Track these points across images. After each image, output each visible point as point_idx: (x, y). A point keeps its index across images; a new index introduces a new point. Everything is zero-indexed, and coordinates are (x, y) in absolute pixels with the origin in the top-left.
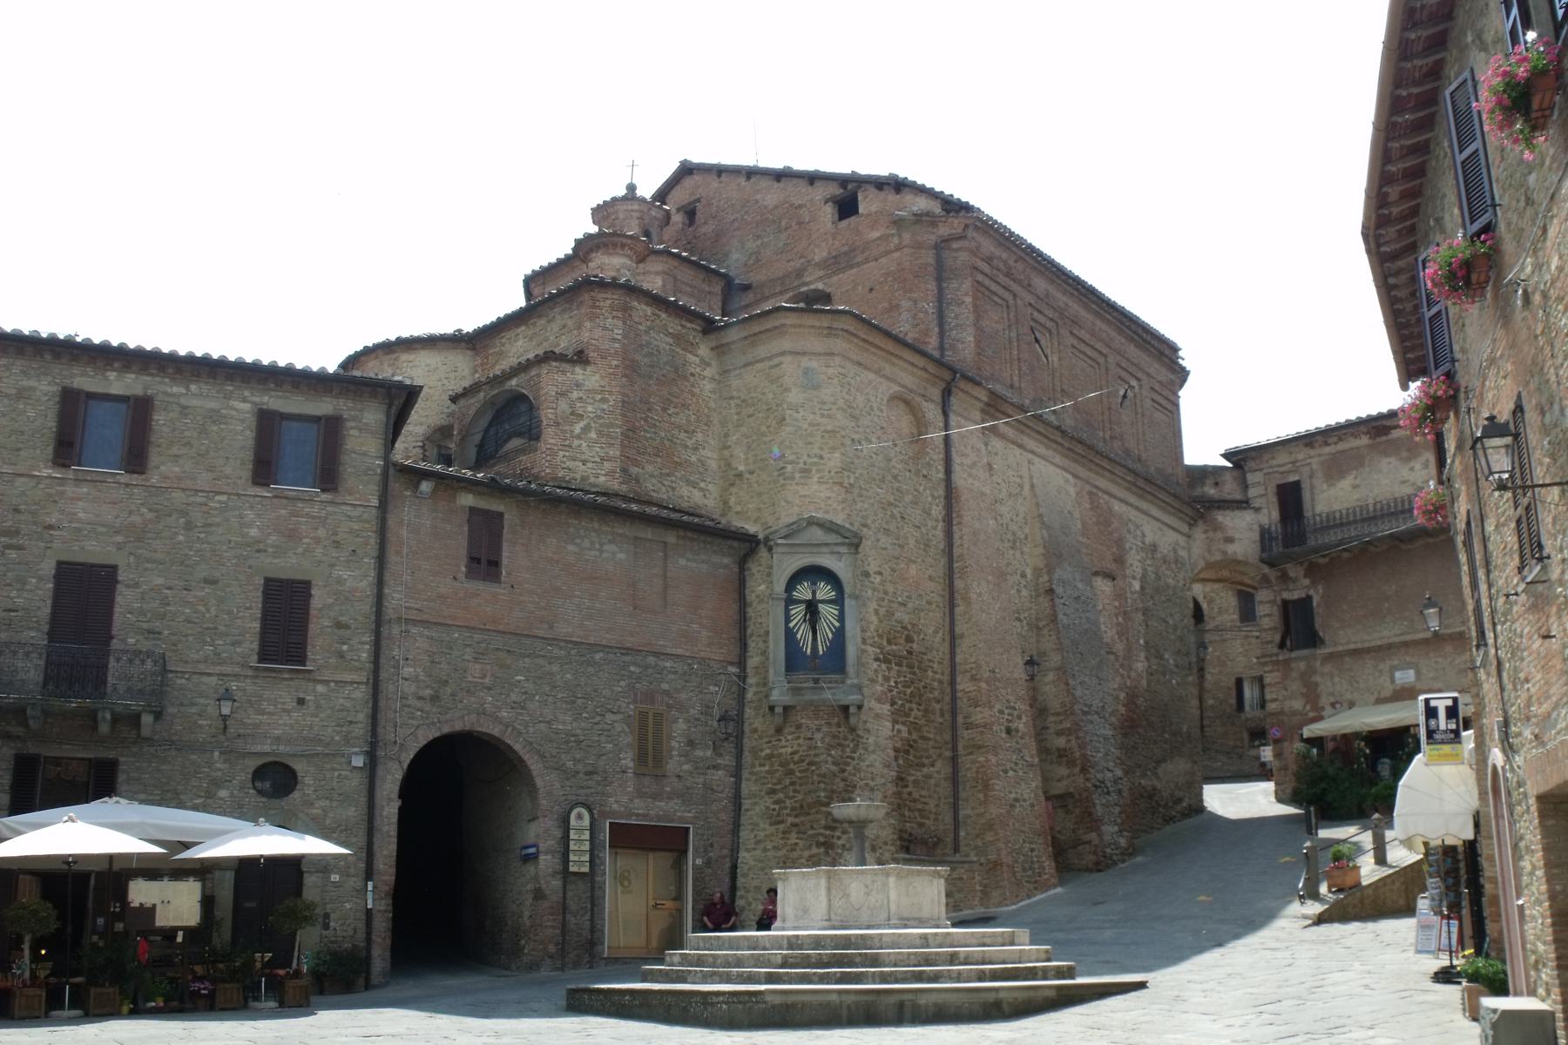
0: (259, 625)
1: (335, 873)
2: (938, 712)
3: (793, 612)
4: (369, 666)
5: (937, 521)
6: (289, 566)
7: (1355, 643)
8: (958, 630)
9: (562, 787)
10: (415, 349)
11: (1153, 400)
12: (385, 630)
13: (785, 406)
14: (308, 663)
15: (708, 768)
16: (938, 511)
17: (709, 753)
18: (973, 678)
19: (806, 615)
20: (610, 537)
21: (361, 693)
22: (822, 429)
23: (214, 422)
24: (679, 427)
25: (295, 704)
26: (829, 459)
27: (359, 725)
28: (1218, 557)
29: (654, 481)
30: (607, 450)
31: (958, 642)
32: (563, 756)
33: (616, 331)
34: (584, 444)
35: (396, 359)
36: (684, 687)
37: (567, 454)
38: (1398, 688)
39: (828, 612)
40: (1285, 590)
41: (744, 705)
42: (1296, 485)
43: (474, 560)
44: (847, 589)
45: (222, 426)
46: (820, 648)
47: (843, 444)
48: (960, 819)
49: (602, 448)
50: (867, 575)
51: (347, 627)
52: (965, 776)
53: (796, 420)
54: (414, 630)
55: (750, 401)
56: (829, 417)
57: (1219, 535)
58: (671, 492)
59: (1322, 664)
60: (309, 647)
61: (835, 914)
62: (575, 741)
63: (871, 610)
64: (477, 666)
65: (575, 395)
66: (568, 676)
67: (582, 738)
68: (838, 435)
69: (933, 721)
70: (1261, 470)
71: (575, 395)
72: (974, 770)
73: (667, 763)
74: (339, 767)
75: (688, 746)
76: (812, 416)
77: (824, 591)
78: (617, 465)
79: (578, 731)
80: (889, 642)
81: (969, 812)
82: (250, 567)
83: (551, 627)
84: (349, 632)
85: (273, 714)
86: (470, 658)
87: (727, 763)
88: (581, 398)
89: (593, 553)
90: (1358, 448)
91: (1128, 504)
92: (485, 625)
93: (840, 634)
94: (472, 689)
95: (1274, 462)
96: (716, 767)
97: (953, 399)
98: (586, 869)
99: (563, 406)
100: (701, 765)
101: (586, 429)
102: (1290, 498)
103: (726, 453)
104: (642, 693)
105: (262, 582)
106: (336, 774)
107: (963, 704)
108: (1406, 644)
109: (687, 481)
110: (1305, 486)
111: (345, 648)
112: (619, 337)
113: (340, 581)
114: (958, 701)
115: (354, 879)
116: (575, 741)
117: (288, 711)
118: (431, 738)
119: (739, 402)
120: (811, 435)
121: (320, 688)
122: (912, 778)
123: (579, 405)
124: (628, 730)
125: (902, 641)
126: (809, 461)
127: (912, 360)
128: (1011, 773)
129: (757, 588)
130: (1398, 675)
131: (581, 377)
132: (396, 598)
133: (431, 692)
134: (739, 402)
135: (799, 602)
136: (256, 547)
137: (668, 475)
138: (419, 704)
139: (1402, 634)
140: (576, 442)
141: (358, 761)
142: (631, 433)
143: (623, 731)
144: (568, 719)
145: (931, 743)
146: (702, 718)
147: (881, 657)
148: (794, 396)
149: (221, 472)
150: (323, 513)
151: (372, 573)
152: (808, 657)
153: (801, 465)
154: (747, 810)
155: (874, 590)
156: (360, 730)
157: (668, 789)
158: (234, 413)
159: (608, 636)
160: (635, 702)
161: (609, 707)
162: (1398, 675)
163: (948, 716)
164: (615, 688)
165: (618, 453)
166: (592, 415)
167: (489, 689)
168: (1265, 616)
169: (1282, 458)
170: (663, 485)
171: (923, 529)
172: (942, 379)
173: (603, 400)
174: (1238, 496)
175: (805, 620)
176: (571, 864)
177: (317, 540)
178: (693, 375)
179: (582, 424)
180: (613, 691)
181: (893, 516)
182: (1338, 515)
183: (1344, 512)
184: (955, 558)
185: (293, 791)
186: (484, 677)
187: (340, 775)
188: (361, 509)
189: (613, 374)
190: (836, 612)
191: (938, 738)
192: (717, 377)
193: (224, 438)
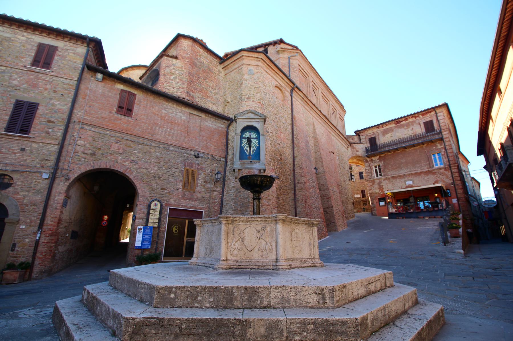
0: (8, 117)
1: (23, 225)
2: (290, 179)
3: (243, 141)
4: (61, 138)
5: (289, 124)
6: (29, 97)
7: (393, 175)
8: (295, 155)
9: (150, 193)
10: (134, 70)
12: (71, 125)
13: (243, 79)
14: (30, 134)
15: (212, 191)
16: (289, 121)
17: (212, 186)
18: (301, 168)
19: (247, 142)
20: (180, 111)
21: (55, 148)
22: (254, 86)
23: (7, 41)
24: (210, 86)
25: (19, 151)
26: (256, 95)
27: (51, 162)
28: (355, 155)
29: (199, 99)
30: (182, 85)
31: (295, 158)
32: (152, 182)
33: (188, 52)
34: (174, 82)
35: (129, 73)
36: (204, 163)
37: (167, 84)
38: (407, 186)
39: (254, 142)
41: (226, 171)
42: (374, 138)
43: (120, 107)
44: (261, 132)
45: (10, 43)
46: (252, 152)
47: (261, 92)
48: (297, 212)
49: (180, 84)
50: (268, 132)
51: (53, 122)
52: (298, 199)
53: (246, 83)
54: (87, 127)
55: (232, 81)
56: (257, 83)
57: (355, 150)
58: (205, 104)
59: (384, 181)
60: (32, 128)
61: (232, 255)
62: (158, 177)
63: (269, 143)
64: (116, 145)
65: (172, 67)
66: (158, 154)
67: (161, 176)
68: (259, 89)
69: (288, 181)
71: (172, 67)
72: (301, 196)
73: (196, 188)
74: (36, 178)
75: (204, 183)
76: (251, 83)
77: (254, 135)
78: (185, 90)
79: (160, 174)
80: (275, 154)
81: (300, 210)
82: (10, 95)
83: (152, 136)
84: (54, 124)
85: (7, 154)
86: (113, 142)
87: (219, 190)
88: (174, 69)
89: (173, 115)
90: (392, 127)
92: (122, 130)
93: (258, 148)
94: (113, 153)
95: (368, 133)
96: (215, 191)
98: (156, 225)
99: (168, 70)
100: (209, 189)
101: (175, 78)
102: (373, 141)
103: (225, 97)
104: (188, 163)
105: (15, 101)
106: (34, 181)
107: (297, 177)
108: (409, 175)
109: (211, 102)
110: (377, 138)
111: (50, 130)
112: (189, 54)
113: (53, 105)
114: (296, 176)
115: (33, 227)
116: (158, 177)
117: (15, 153)
118: (88, 169)
119: (229, 82)
120: (251, 88)
121: (34, 145)
122: (282, 198)
123: (173, 70)
124: (181, 175)
125: (279, 155)
126: (250, 95)
127: (282, 77)
128: (313, 198)
129: (231, 134)
130: (407, 182)
131: (175, 63)
132: (78, 114)
133: (91, 152)
134: (229, 82)
135: (245, 138)
136: (16, 88)
137: (205, 99)
138: (84, 156)
139: (408, 172)
140: (171, 81)
141: (45, 176)
142: (191, 82)
143: (179, 175)
144: (156, 168)
145: (288, 188)
146: (211, 174)
147: (272, 158)
148: (246, 77)
149: (6, 59)
150: (51, 80)
151: (70, 104)
152: (248, 155)
153: (247, 96)
154: (225, 206)
155: (270, 137)
156: (51, 163)
157: (195, 197)
158: (17, 40)
159: (176, 142)
160: (185, 166)
161: (174, 166)
162: (407, 182)
163: (292, 180)
164: (177, 160)
165: (186, 87)
166: (178, 74)
167: (121, 154)
169: (370, 132)
170: (203, 101)
171: (285, 125)
172: (291, 87)
173: (182, 70)
174: (358, 142)
175: (247, 144)
176: (149, 223)
177: (46, 89)
178: (215, 73)
179: (174, 76)
180: (176, 161)
181: (276, 118)
182: (392, 142)
183: (388, 142)
184: (294, 135)
185: (10, 187)
186: (119, 149)
187: (36, 181)
188: (69, 81)
189: (186, 63)
190: (257, 142)
191: (290, 187)
192: (223, 76)
193: (10, 48)
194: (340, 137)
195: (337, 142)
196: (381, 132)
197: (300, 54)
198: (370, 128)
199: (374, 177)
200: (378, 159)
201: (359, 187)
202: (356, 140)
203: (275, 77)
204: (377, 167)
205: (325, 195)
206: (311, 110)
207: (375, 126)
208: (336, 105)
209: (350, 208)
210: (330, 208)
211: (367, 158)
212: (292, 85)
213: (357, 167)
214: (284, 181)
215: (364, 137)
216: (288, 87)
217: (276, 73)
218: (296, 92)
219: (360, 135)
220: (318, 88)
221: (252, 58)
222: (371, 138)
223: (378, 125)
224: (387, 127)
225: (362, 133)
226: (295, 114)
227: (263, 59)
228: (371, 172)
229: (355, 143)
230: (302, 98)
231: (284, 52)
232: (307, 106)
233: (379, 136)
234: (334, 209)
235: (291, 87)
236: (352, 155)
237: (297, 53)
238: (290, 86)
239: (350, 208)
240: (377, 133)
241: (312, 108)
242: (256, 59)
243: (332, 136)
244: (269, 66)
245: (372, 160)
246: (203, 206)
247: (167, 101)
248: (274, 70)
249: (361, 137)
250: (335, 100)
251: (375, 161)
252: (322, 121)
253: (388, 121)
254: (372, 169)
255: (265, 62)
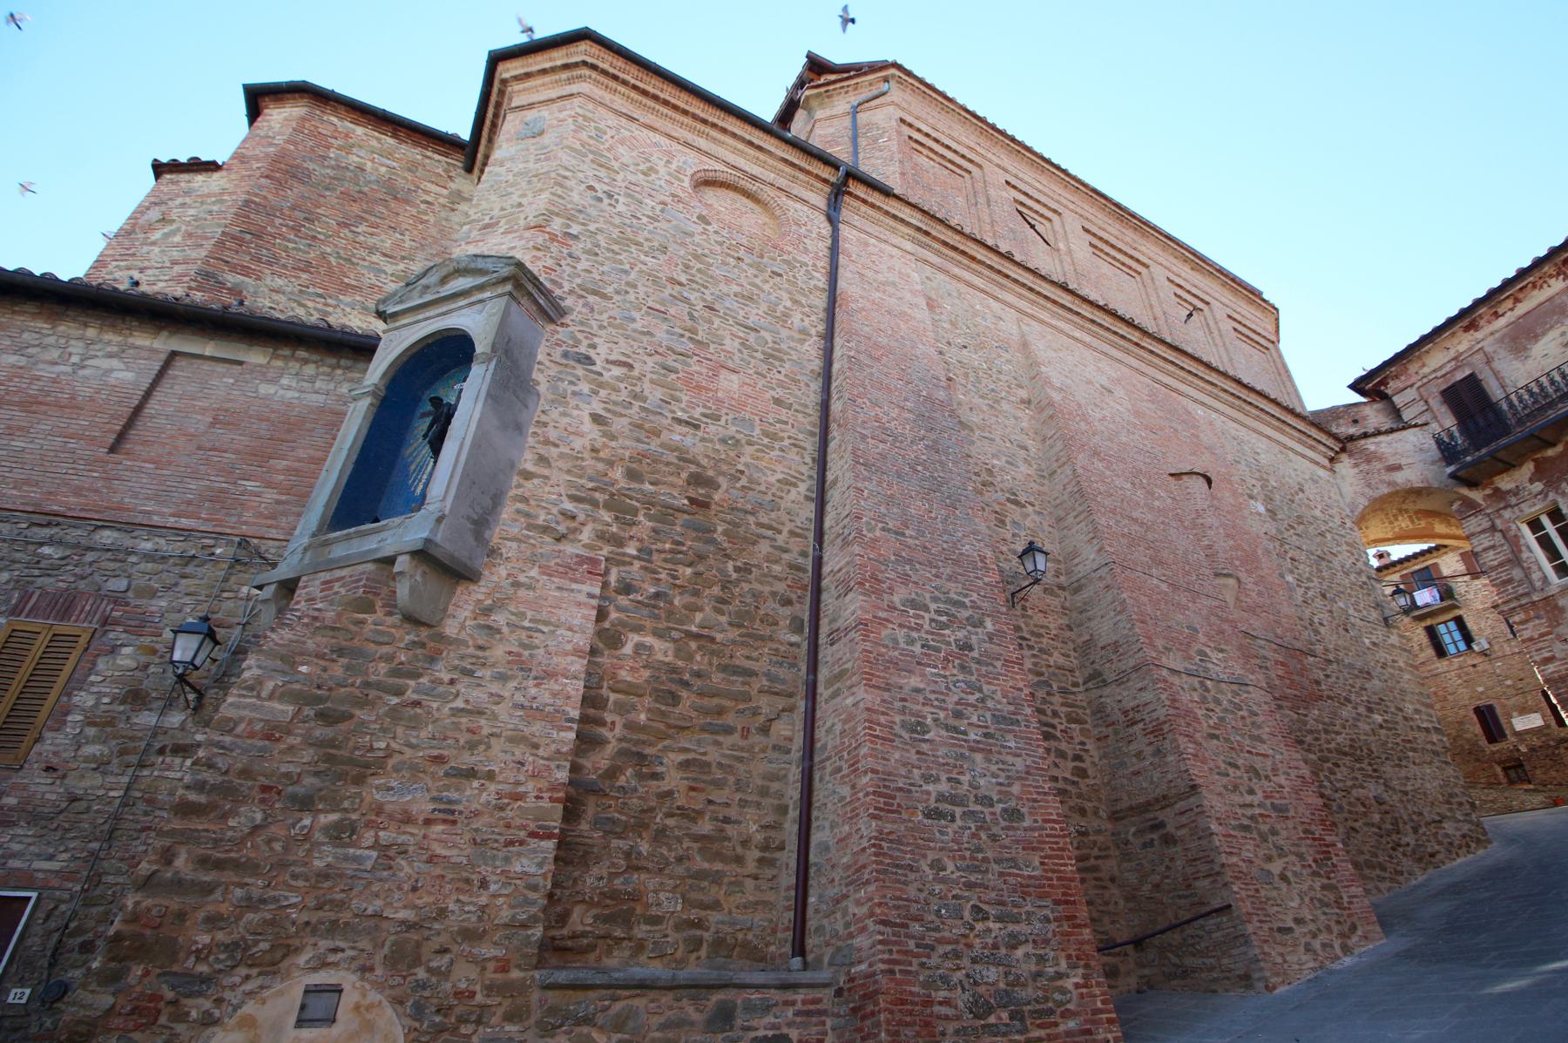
11: (1235, 329)
28: (1385, 490)
40: (1505, 508)
42: (1472, 382)
57: (1377, 465)
70: (1412, 386)
90: (1550, 299)
91: (1210, 407)
95: (1426, 370)
97: (845, 214)
127: (748, 137)
168: (1485, 550)
169: (1436, 360)
172: (825, 181)
194: (1254, 411)
195: (1243, 433)
196: (1501, 340)
197: (900, 82)
198: (1425, 340)
199: (1545, 579)
200: (1531, 481)
201: (1522, 675)
202: (1374, 417)
203: (702, 143)
204: (1545, 520)
205: (1136, 709)
206: (1002, 286)
207: (1450, 323)
208: (1196, 282)
209: (1432, 786)
210: (1182, 797)
211: (1465, 491)
212: (826, 172)
213: (1477, 582)
214: (719, 637)
215: (1411, 394)
216: (811, 188)
217: (704, 122)
218: (864, 201)
219: (1389, 392)
220: (1055, 211)
221: (547, 79)
222: (1453, 386)
223: (1464, 313)
224: (1522, 309)
225: (1397, 377)
226: (847, 283)
227: (594, 67)
228: (1515, 559)
229: (1365, 436)
230: (919, 229)
231: (828, 97)
232: (968, 268)
233: (1496, 365)
234: (1214, 801)
235: (825, 181)
236: (1367, 490)
237: (886, 80)
238: (817, 177)
239: (1432, 786)
240: (1480, 356)
241: (1007, 276)
242: (564, 75)
243: (1191, 406)
244: (645, 93)
245: (1498, 494)
246: (51, 858)
247: (54, 318)
248: (685, 112)
249: (1398, 400)
250: (1186, 260)
251: (1516, 492)
252: (1089, 332)
253: (1511, 274)
254: (1515, 542)
255: (615, 78)
